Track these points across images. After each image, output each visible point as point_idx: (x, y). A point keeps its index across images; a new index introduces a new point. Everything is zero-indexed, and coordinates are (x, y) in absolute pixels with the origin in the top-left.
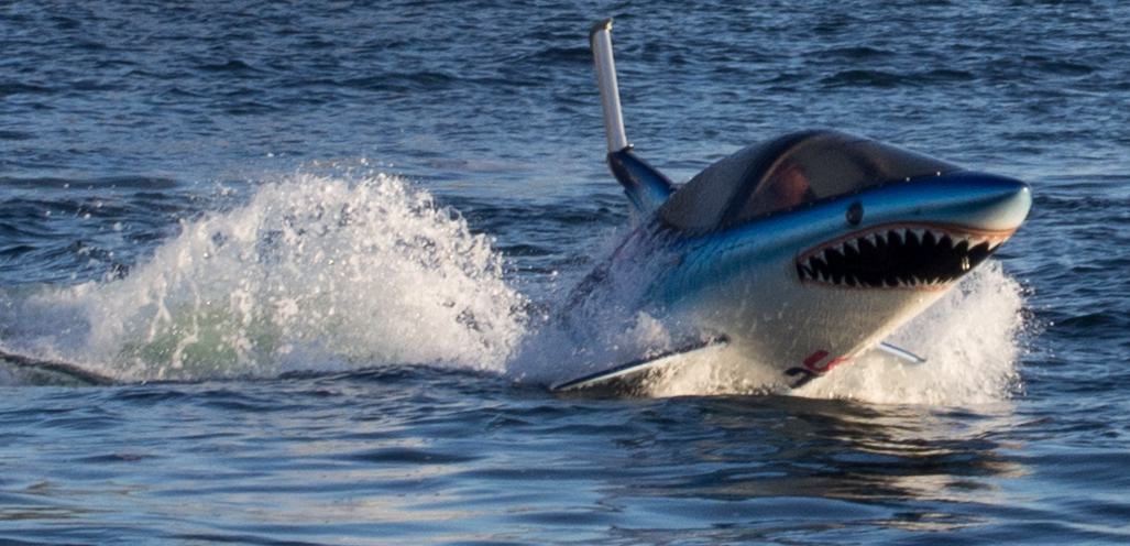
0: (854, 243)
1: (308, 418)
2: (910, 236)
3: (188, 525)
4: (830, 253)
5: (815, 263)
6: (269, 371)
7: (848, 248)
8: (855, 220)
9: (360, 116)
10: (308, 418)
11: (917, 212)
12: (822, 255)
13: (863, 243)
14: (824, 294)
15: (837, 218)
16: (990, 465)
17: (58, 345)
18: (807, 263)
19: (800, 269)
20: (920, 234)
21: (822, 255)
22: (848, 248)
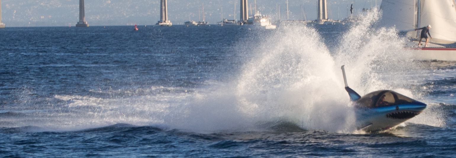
0: (397, 113)
1: (59, 148)
2: (407, 112)
3: (8, 155)
4: (393, 114)
5: (390, 115)
6: (332, 143)
7: (396, 113)
8: (397, 109)
9: (435, 144)
10: (59, 148)
11: (408, 109)
12: (391, 114)
13: (399, 113)
14: (390, 119)
15: (394, 108)
16: (273, 131)
17: (366, 112)
18: (389, 115)
19: (387, 116)
20: (403, 112)
21: (391, 114)
22: (396, 113)
